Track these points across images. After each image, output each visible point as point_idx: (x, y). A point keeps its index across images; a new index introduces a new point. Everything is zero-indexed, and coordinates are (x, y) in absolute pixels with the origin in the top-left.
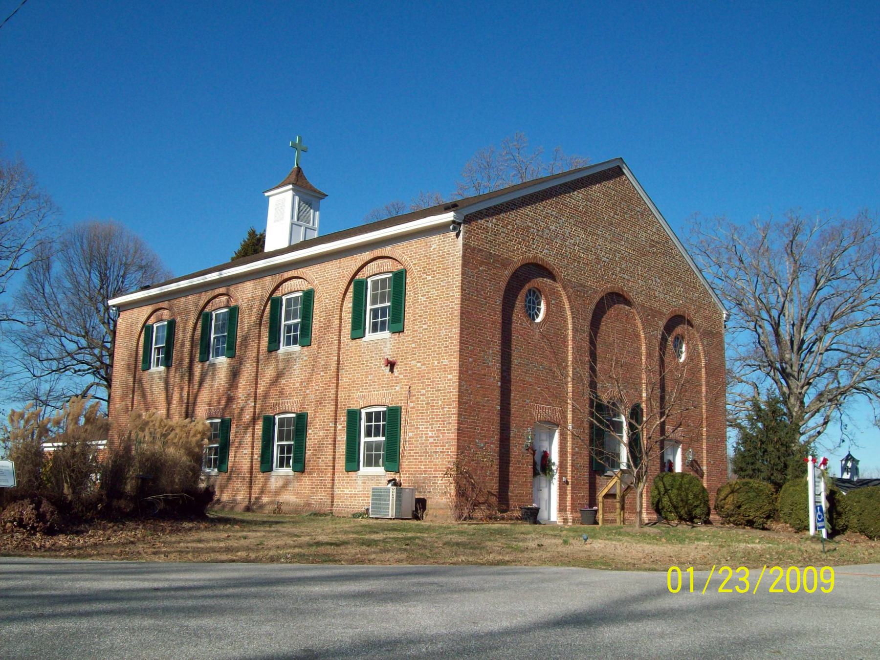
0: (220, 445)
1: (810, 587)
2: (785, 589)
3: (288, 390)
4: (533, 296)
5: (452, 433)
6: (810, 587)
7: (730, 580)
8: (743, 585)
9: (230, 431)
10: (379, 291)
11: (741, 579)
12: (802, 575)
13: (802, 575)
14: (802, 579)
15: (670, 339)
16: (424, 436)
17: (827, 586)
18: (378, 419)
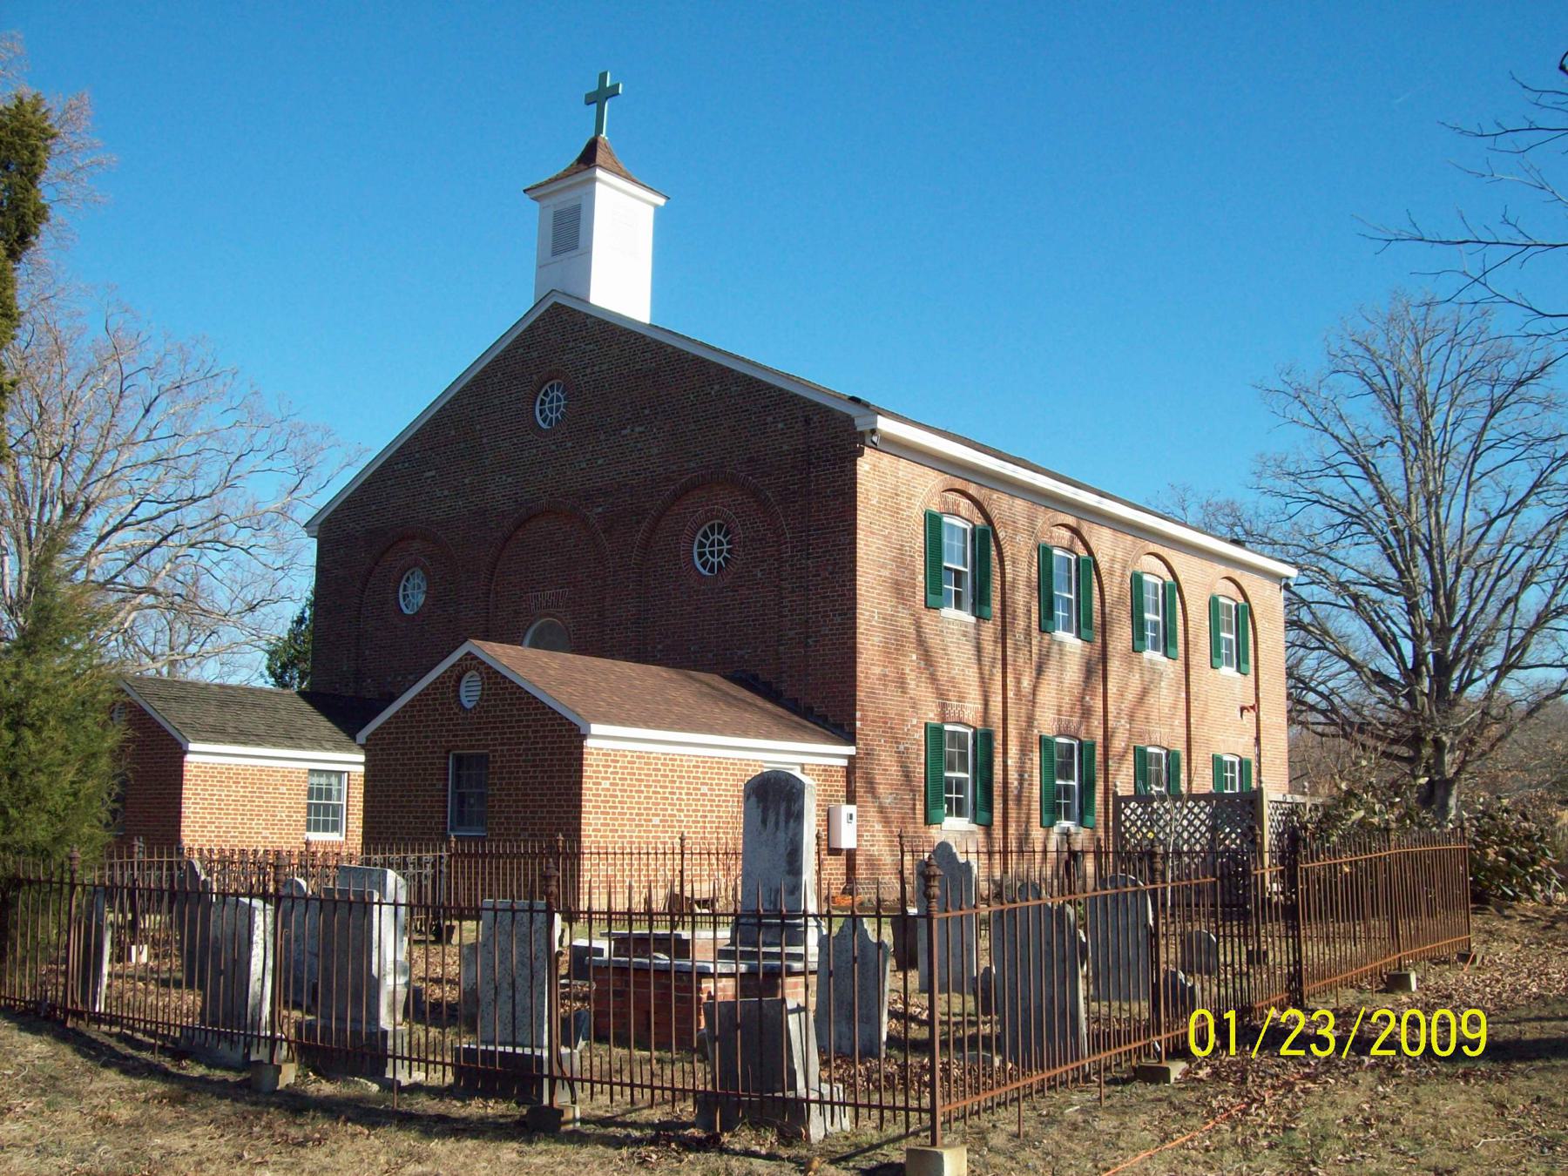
0: (545, 1107)
1: (1444, 1047)
2: (1400, 1051)
3: (1154, 715)
4: (713, 563)
5: (591, 765)
6: (1444, 1047)
7: (1301, 1034)
8: (1323, 1043)
9: (745, 791)
10: (954, 796)
11: (1320, 1032)
12: (1429, 1025)
13: (1429, 1025)
14: (1429, 1035)
15: (984, 963)
16: (684, 797)
17: (1474, 1045)
18: (326, 823)
